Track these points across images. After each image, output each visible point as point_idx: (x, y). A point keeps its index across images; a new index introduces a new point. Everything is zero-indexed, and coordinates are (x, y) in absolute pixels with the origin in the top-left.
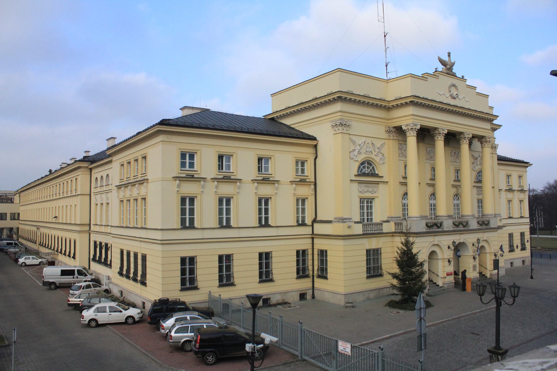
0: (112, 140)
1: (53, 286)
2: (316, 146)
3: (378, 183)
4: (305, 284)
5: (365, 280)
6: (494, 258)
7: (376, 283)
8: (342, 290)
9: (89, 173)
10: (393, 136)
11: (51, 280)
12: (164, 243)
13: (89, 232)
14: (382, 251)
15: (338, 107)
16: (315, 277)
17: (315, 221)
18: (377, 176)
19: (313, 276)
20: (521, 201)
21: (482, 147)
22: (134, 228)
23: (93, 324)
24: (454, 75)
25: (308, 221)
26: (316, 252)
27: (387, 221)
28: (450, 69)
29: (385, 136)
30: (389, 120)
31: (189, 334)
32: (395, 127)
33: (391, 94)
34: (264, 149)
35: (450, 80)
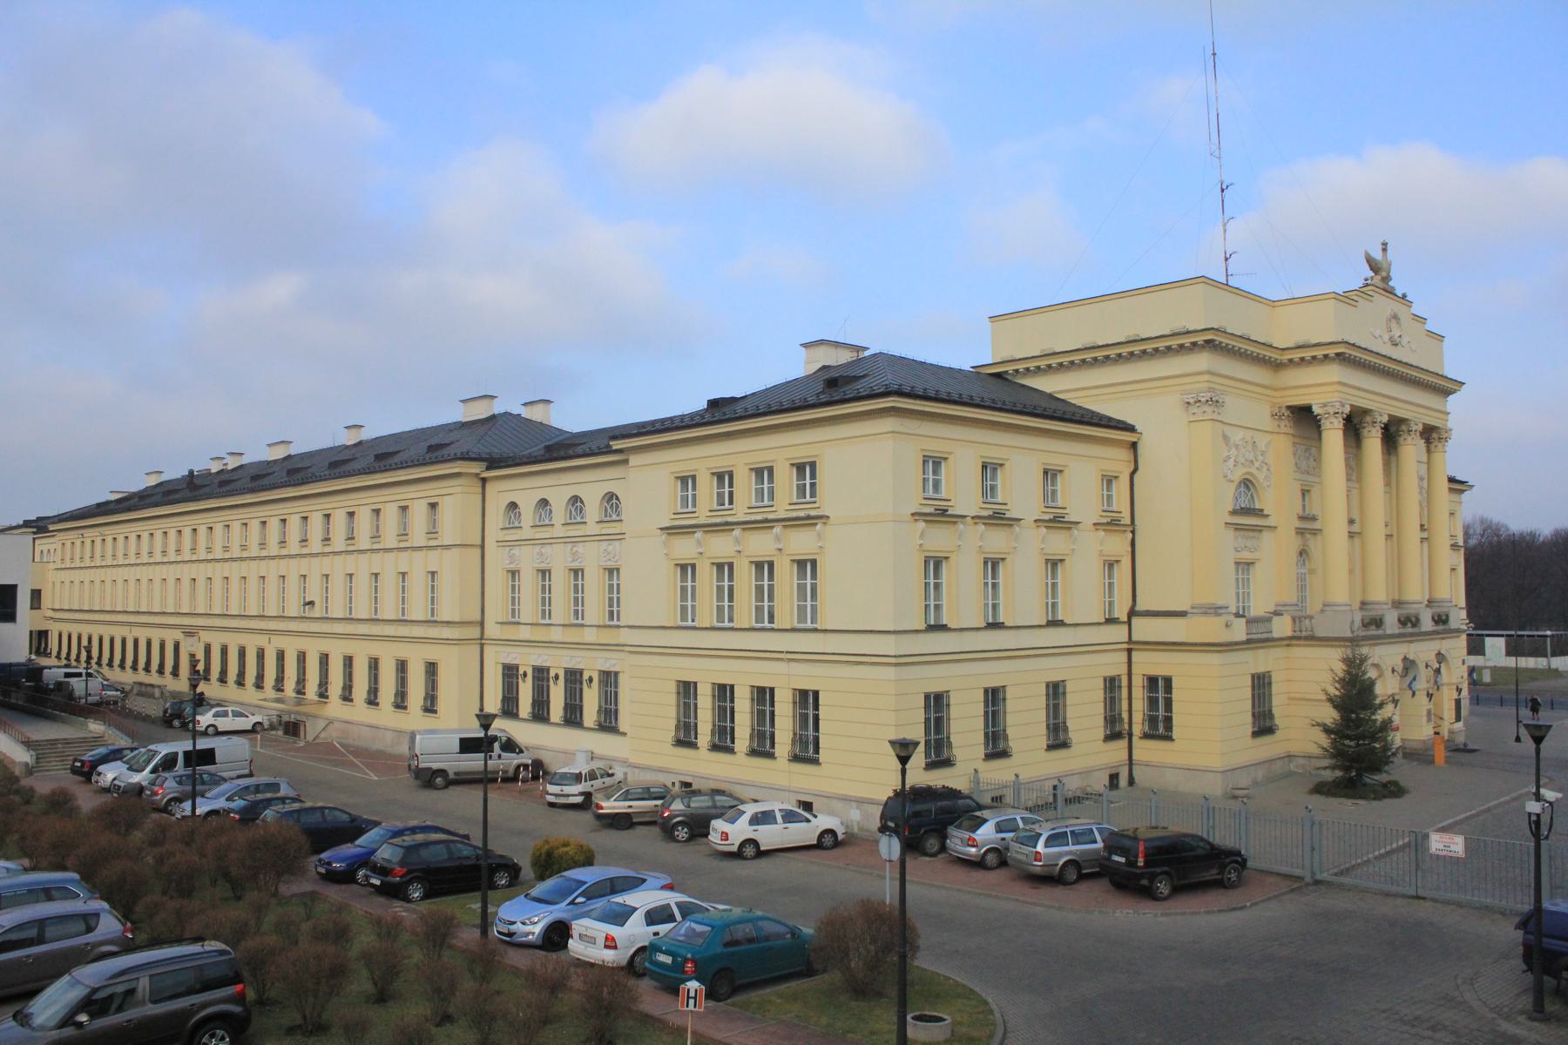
0: (485, 402)
1: (439, 780)
2: (1134, 445)
3: (1258, 529)
4: (1118, 751)
5: (1249, 741)
6: (1455, 695)
7: (1268, 748)
8: (1217, 763)
9: (480, 490)
10: (1286, 426)
11: (435, 766)
12: (902, 661)
13: (482, 642)
14: (1008, 696)
15: (1202, 361)
16: (1135, 739)
17: (1132, 613)
18: (1259, 513)
19: (1130, 735)
20: (1111, 565)
21: (1429, 451)
22: (793, 630)
23: (749, 851)
24: (1390, 292)
25: (1121, 612)
26: (1138, 682)
27: (1276, 613)
28: (1387, 279)
29: (1268, 423)
30: (1276, 390)
31: (1071, 848)
32: (1289, 407)
33: (1283, 333)
34: (994, 444)
35: (1384, 305)
